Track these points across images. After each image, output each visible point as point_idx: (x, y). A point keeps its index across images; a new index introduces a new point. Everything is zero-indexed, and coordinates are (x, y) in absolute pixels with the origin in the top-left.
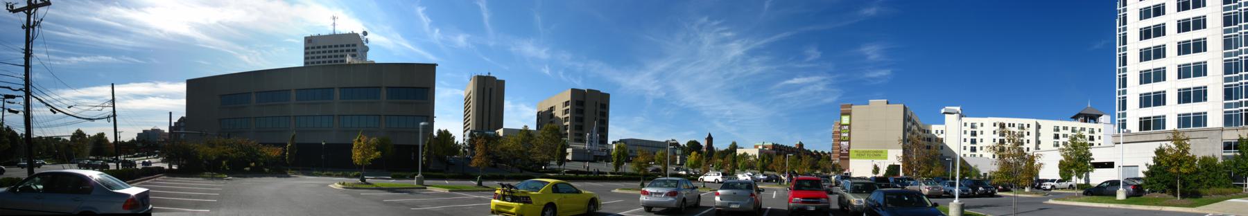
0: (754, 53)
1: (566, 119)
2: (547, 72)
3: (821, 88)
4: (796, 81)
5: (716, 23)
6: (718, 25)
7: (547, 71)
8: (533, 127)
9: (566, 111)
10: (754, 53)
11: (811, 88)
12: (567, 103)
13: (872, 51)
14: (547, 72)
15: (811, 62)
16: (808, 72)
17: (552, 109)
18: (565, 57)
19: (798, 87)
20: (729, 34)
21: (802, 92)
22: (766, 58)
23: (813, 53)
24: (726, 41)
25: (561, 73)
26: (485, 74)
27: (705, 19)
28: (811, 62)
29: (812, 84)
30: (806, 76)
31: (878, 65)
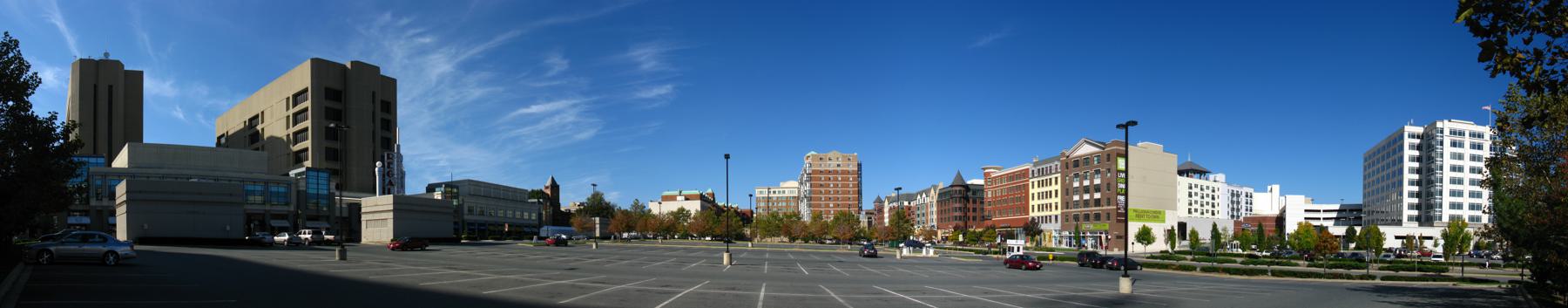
0: (468, 67)
1: (299, 136)
2: (181, 116)
3: (571, 119)
4: (534, 109)
5: (405, 21)
6: (409, 26)
7: (179, 114)
8: (266, 135)
9: (297, 118)
10: (468, 67)
11: (557, 119)
12: (298, 97)
13: (646, 56)
14: (181, 116)
15: (554, 78)
16: (555, 93)
17: (254, 120)
18: (200, 91)
19: (536, 119)
20: (427, 40)
21: (543, 126)
22: (485, 75)
23: (557, 62)
24: (423, 51)
25: (199, 116)
26: (97, 56)
27: (387, 17)
28: (554, 78)
29: (558, 112)
30: (549, 100)
31: (656, 78)
